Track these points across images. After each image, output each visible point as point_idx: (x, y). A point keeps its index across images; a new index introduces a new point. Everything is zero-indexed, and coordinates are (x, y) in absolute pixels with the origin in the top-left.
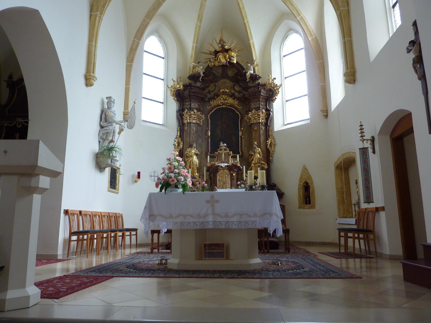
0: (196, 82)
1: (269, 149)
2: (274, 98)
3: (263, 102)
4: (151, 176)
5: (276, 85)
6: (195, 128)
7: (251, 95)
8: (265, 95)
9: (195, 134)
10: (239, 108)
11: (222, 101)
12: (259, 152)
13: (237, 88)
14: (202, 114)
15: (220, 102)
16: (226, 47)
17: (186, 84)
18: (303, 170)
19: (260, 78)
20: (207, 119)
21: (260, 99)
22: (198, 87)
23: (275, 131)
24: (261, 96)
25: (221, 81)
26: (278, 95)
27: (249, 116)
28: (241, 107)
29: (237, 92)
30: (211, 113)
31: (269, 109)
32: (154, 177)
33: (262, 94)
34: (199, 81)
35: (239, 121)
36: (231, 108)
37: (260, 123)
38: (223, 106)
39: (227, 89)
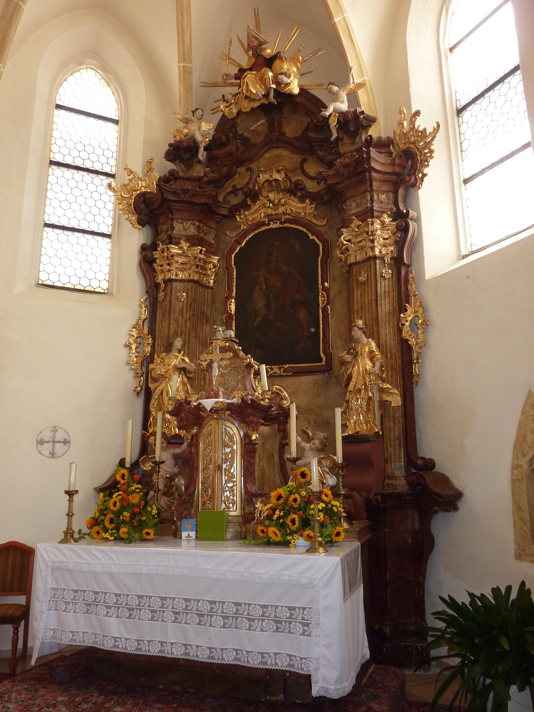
0: (189, 167)
1: (407, 340)
2: (420, 175)
3: (383, 192)
4: (41, 442)
5: (421, 132)
6: (184, 294)
7: (343, 174)
8: (387, 171)
9: (184, 310)
10: (317, 223)
11: (270, 211)
12: (371, 352)
13: (312, 169)
14: (206, 251)
15: (262, 215)
16: (269, 51)
17: (165, 175)
18: (527, 408)
19: (371, 120)
20: (228, 268)
21: (374, 184)
22: (199, 179)
23: (428, 280)
24: (373, 174)
25: (267, 155)
26: (431, 162)
27: (342, 243)
28: (324, 219)
29: (312, 178)
30: (238, 249)
31: (405, 211)
32: (50, 445)
33: (374, 165)
34: (199, 162)
35: (319, 264)
36: (294, 226)
37: (375, 258)
38: (273, 226)
39: (278, 171)
